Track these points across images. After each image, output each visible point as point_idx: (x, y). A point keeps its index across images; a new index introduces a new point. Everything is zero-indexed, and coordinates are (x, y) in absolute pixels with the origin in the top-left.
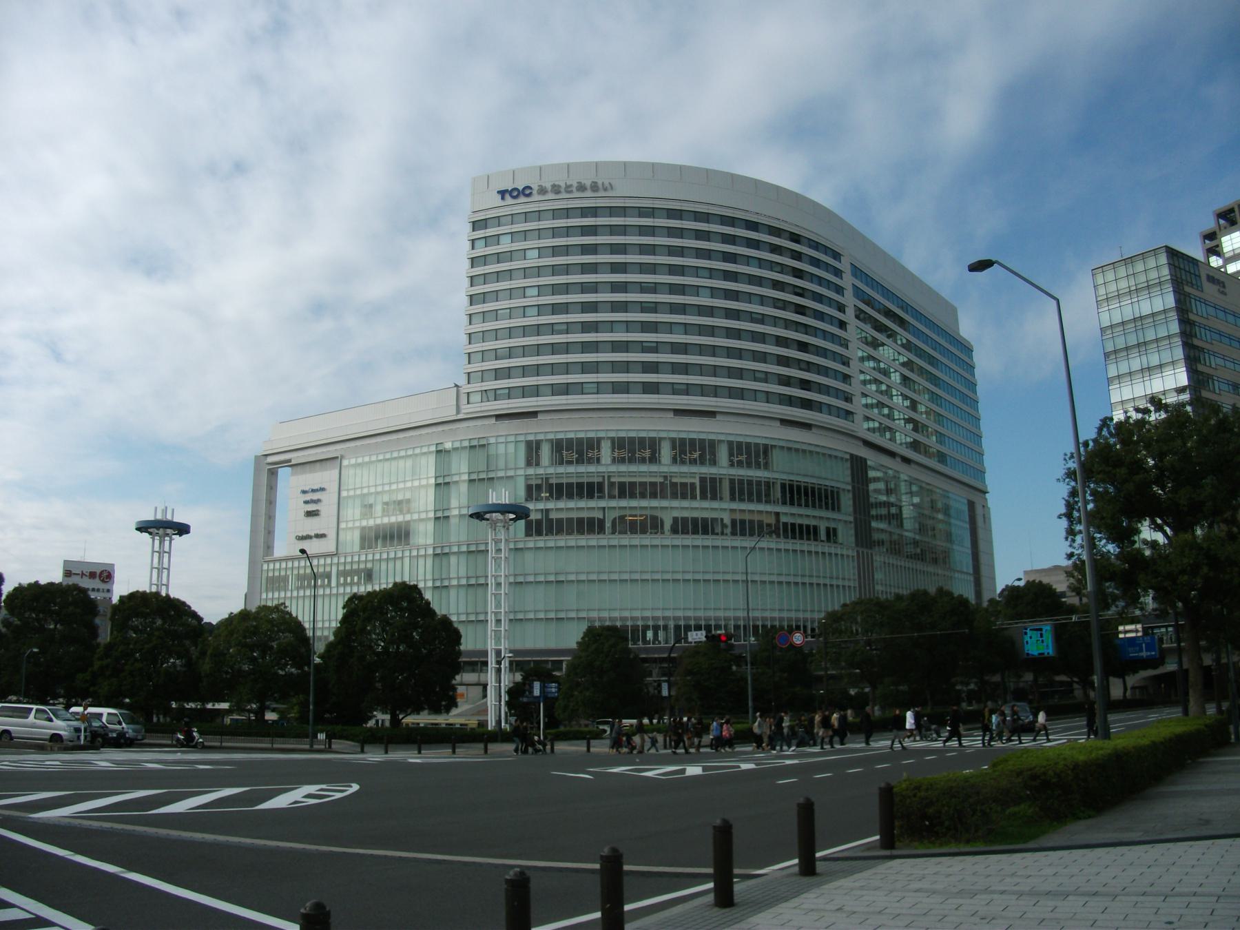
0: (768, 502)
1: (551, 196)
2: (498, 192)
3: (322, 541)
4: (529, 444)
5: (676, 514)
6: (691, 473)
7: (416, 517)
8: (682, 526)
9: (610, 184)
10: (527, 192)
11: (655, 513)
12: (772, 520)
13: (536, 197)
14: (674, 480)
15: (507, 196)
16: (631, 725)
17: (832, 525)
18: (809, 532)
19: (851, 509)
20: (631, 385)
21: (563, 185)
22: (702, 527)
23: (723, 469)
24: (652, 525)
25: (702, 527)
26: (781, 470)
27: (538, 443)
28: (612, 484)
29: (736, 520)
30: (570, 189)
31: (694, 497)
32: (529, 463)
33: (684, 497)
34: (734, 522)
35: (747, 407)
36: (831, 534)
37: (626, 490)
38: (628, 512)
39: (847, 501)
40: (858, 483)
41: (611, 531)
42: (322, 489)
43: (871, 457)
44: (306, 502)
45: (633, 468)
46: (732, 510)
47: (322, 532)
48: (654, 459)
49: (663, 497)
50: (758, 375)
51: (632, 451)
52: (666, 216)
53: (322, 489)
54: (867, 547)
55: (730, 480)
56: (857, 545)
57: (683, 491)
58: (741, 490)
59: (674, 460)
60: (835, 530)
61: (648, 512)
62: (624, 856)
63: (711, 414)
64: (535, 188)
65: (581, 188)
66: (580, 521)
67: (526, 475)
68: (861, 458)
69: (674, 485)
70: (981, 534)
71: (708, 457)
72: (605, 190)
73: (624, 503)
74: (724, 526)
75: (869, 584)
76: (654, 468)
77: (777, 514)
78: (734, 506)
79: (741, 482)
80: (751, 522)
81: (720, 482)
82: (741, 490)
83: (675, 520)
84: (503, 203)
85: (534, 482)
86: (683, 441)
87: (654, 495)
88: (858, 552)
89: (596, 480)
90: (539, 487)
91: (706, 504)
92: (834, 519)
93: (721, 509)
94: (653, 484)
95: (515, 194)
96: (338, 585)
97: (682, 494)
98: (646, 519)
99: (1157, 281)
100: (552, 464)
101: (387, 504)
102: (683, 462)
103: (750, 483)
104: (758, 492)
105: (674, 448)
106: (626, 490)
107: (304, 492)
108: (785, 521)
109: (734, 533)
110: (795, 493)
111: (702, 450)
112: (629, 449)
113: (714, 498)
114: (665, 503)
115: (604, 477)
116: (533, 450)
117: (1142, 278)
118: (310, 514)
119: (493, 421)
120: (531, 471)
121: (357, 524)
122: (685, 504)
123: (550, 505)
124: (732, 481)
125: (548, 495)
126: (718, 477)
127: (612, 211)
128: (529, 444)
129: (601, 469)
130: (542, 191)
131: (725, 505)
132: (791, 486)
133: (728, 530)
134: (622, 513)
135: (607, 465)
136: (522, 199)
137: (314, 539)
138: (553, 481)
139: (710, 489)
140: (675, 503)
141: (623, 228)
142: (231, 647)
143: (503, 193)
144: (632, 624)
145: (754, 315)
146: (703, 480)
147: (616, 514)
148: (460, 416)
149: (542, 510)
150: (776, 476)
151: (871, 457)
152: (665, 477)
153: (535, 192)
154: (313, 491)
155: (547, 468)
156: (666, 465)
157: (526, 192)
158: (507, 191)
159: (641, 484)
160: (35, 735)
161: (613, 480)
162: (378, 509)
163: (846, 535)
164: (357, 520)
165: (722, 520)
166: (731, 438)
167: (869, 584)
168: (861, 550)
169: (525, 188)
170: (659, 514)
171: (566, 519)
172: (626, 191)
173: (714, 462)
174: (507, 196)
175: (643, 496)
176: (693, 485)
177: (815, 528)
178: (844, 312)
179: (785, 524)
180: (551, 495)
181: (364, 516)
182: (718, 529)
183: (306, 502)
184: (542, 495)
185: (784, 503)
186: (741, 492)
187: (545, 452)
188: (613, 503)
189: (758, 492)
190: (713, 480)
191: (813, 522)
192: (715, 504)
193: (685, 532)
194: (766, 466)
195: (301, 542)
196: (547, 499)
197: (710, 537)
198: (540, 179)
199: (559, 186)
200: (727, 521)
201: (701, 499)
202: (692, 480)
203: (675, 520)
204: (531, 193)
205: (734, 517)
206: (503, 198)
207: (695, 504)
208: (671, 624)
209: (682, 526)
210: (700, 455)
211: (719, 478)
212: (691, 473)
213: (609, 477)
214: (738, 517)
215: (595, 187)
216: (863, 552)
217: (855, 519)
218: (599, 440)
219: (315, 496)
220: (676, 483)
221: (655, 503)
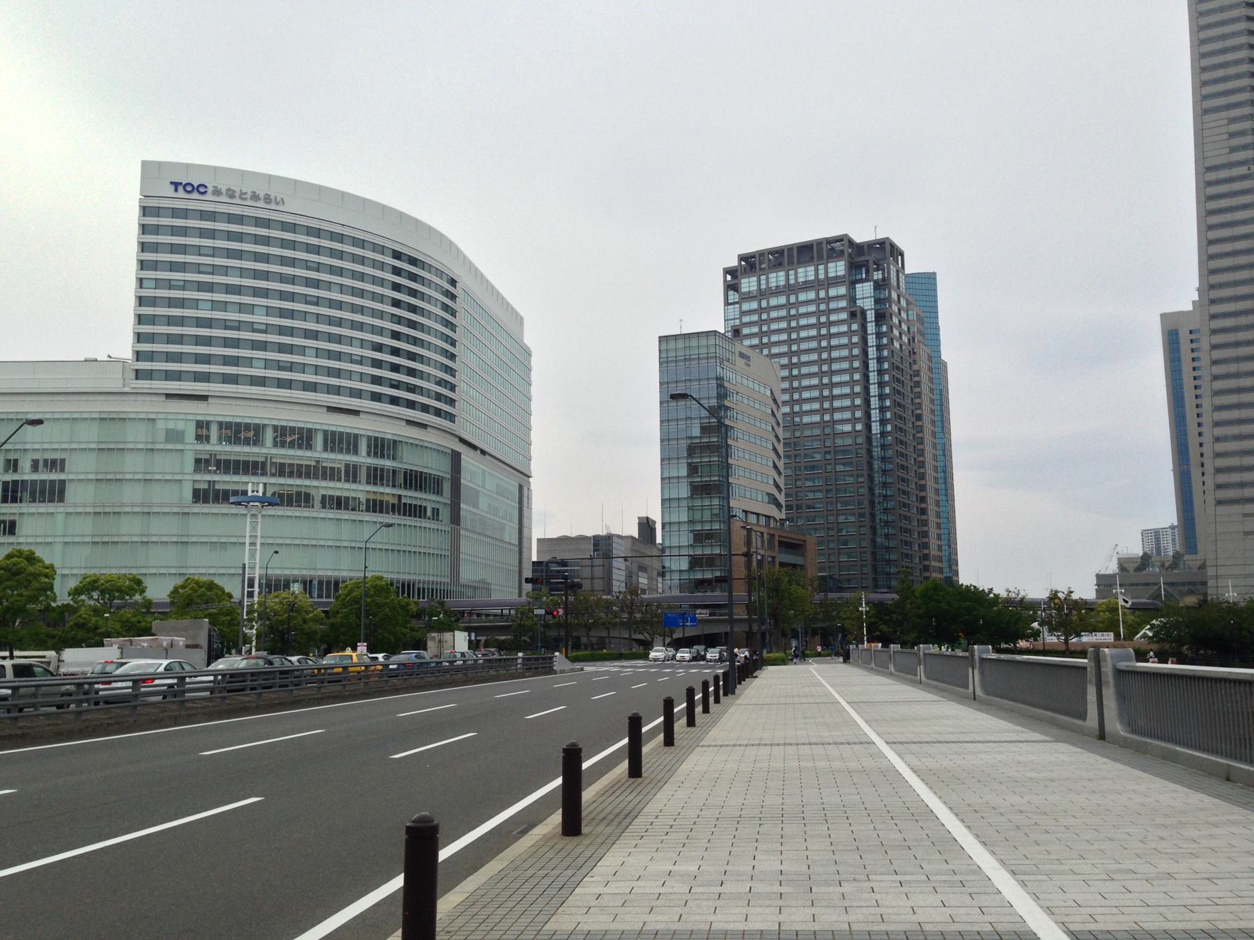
0: (394, 486)
1: (224, 199)
5: (323, 492)
6: (338, 459)
7: (72, 477)
9: (282, 199)
10: (202, 190)
11: (308, 491)
12: (396, 501)
13: (209, 197)
15: (180, 189)
18: (416, 511)
19: (449, 496)
20: (182, 373)
22: (339, 503)
23: (363, 459)
24: (303, 499)
25: (339, 503)
26: (410, 461)
30: (245, 197)
31: (339, 480)
33: (332, 479)
34: (368, 500)
36: (436, 512)
37: (282, 470)
39: (447, 488)
45: (237, 449)
49: (316, 478)
51: (237, 432)
56: (451, 523)
57: (330, 474)
58: (376, 476)
60: (438, 509)
62: (583, 750)
63: (356, 413)
65: (255, 197)
69: (324, 468)
72: (277, 203)
73: (282, 481)
76: (308, 453)
77: (400, 496)
79: (375, 469)
80: (381, 502)
82: (376, 476)
83: (324, 497)
84: (173, 194)
86: (284, 428)
87: (308, 476)
90: (207, 462)
91: (347, 486)
92: (425, 499)
93: (360, 490)
94: (308, 466)
97: (322, 475)
99: (674, 359)
102: (283, 445)
106: (282, 470)
109: (368, 510)
110: (415, 480)
111: (346, 442)
112: (285, 436)
113: (355, 481)
114: (315, 483)
115: (266, 458)
116: (202, 427)
117: (672, 354)
122: (332, 484)
124: (369, 468)
127: (285, 226)
128: (199, 424)
129: (264, 451)
130: (217, 192)
131: (361, 487)
133: (364, 507)
135: (213, 445)
136: (195, 195)
139: (351, 473)
140: (324, 484)
142: (566, 613)
143: (176, 185)
146: (347, 466)
148: (127, 389)
150: (400, 465)
152: (318, 462)
155: (216, 447)
156: (317, 453)
157: (200, 189)
158: (181, 184)
159: (289, 464)
160: (936, 687)
164: (707, 521)
169: (200, 185)
170: (313, 492)
172: (294, 208)
173: (356, 452)
174: (180, 189)
175: (300, 476)
178: (455, 347)
179: (405, 504)
185: (405, 488)
186: (375, 477)
190: (355, 466)
192: (354, 486)
193: (206, 501)
196: (215, 472)
198: (215, 180)
199: (234, 191)
200: (363, 500)
203: (324, 497)
204: (206, 192)
205: (369, 497)
206: (176, 190)
207: (339, 485)
210: (298, 439)
212: (338, 459)
215: (268, 199)
218: (264, 426)
220: (327, 467)
221: (307, 482)
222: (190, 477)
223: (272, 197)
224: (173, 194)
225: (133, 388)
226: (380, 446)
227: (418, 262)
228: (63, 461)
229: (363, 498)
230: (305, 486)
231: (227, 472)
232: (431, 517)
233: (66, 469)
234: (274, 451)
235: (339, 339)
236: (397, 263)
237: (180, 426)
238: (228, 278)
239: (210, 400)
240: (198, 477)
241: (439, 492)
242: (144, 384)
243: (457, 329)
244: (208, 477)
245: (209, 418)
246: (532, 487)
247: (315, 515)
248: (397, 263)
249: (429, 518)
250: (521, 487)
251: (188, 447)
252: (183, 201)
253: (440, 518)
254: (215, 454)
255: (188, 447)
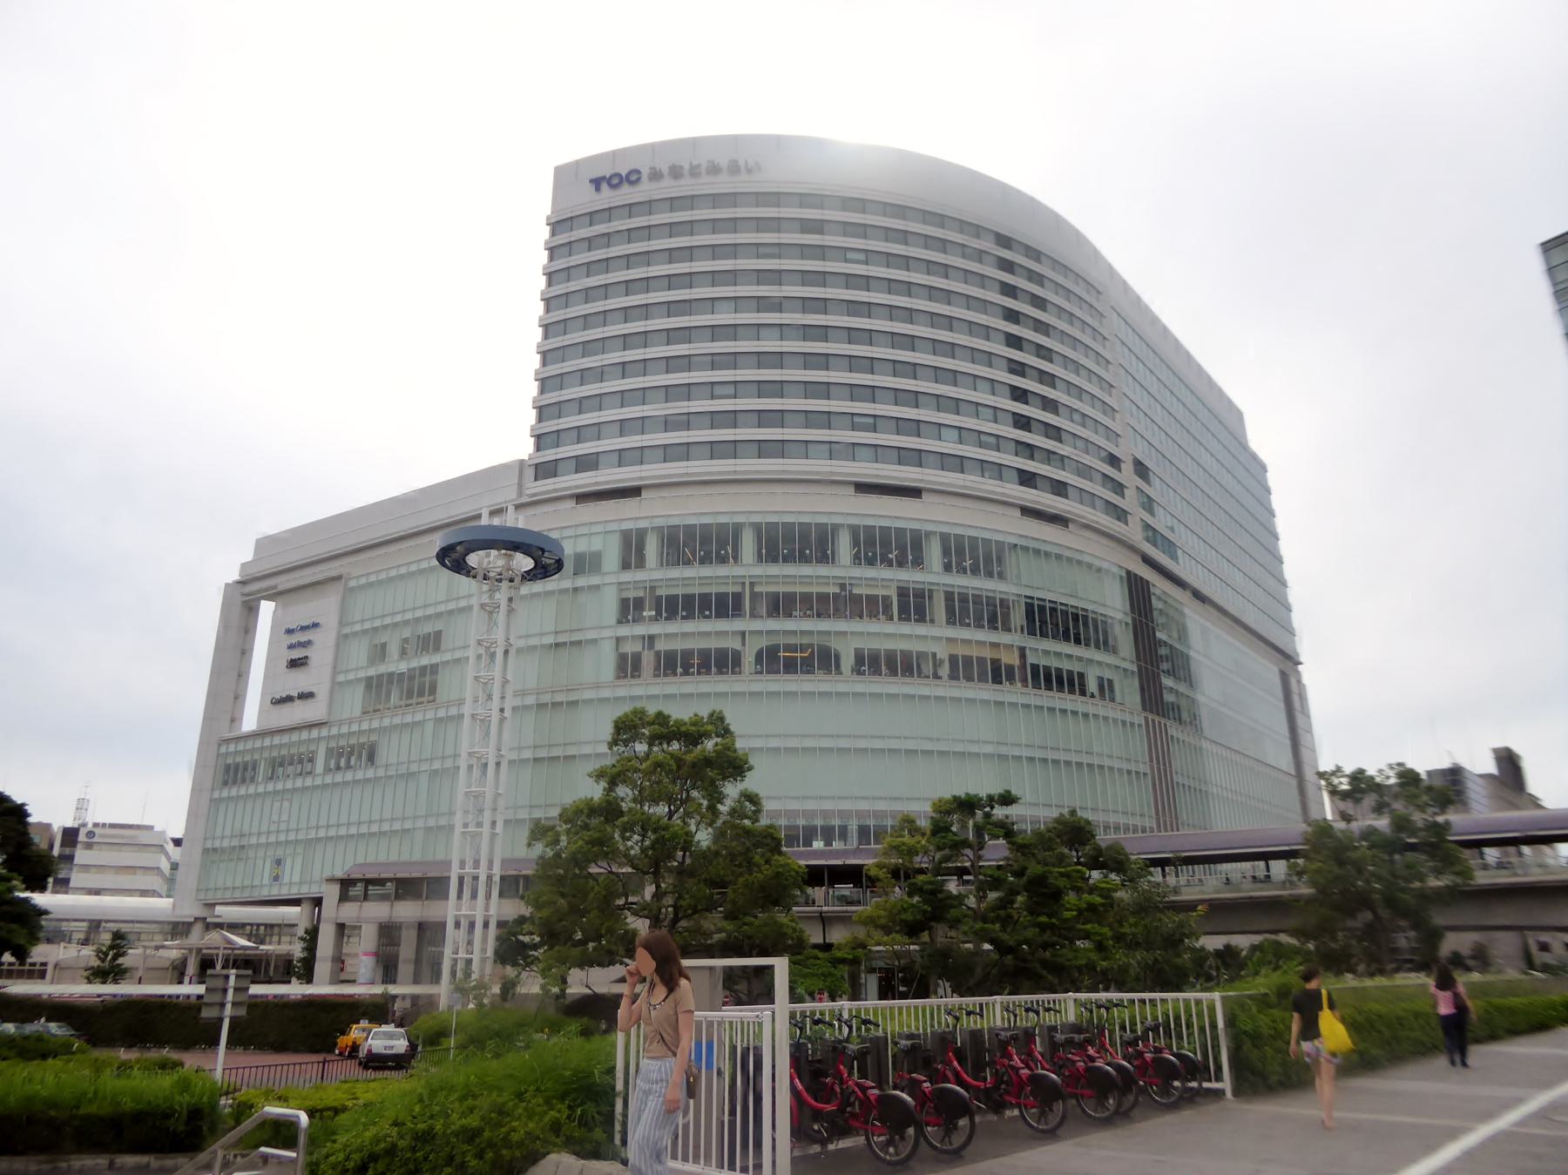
1: (667, 182)
2: (591, 181)
3: (309, 702)
4: (626, 536)
6: (884, 579)
7: (448, 657)
8: (869, 663)
10: (633, 178)
14: (856, 591)
15: (604, 186)
16: (907, 1046)
17: (1107, 674)
18: (1070, 683)
21: (687, 167)
22: (903, 665)
24: (823, 660)
25: (903, 665)
27: (641, 534)
28: (755, 596)
29: (957, 656)
32: (626, 566)
34: (953, 659)
35: (968, 484)
36: (1105, 688)
37: (780, 605)
38: (782, 641)
39: (1124, 639)
40: (1140, 615)
41: (753, 670)
42: (315, 625)
43: (1159, 584)
44: (291, 647)
46: (949, 640)
47: (306, 690)
48: (825, 557)
50: (967, 251)
52: (896, 461)
53: (315, 625)
54: (1164, 716)
55: (946, 593)
56: (1144, 709)
57: (873, 607)
58: (960, 609)
59: (857, 559)
61: (815, 640)
63: (914, 492)
64: (645, 172)
66: (705, 655)
67: (620, 583)
68: (1141, 578)
70: (1304, 739)
71: (910, 557)
74: (937, 664)
75: (1165, 771)
76: (822, 570)
78: (952, 632)
81: (930, 597)
85: (631, 594)
88: (1146, 719)
89: (731, 589)
90: (639, 604)
95: (615, 181)
96: (327, 770)
98: (812, 653)
100: (662, 565)
101: (406, 641)
103: (977, 599)
104: (993, 614)
105: (856, 543)
106: (780, 605)
107: (289, 631)
108: (1035, 662)
109: (954, 676)
113: (921, 618)
115: (744, 584)
118: (294, 664)
119: (570, 504)
120: (627, 577)
121: (362, 674)
123: (656, 629)
124: (949, 597)
125: (654, 613)
126: (927, 587)
128: (626, 536)
132: (1042, 609)
134: (772, 641)
136: (626, 188)
137: (298, 702)
138: (662, 592)
139: (913, 605)
141: (825, 387)
144: (787, 823)
145: (983, 438)
147: (764, 643)
149: (644, 637)
150: (1014, 590)
151: (1159, 584)
152: (843, 586)
153: (645, 177)
154: (304, 628)
155: (657, 574)
156: (844, 569)
157: (632, 178)
158: (603, 178)
161: (757, 589)
162: (394, 650)
163: (1129, 692)
165: (934, 655)
166: (945, 529)
167: (1165, 771)
168: (1150, 717)
170: (835, 644)
171: (634, 598)
173: (918, 562)
174: (604, 186)
176: (886, 599)
177: (1081, 676)
179: (1035, 668)
180: (659, 613)
181: (372, 662)
182: (928, 668)
183: (291, 647)
184: (645, 614)
186: (965, 612)
187: (652, 548)
188: (757, 625)
189: (993, 614)
190: (920, 594)
191: (1076, 668)
192: (921, 630)
194: (1001, 576)
195: (279, 706)
196: (656, 619)
197: (915, 680)
201: (900, 619)
202: (885, 592)
204: (638, 180)
206: (598, 189)
207: (890, 628)
208: (853, 826)
209: (869, 663)
211: (929, 590)
212: (884, 579)
213: (752, 584)
214: (961, 651)
216: (1160, 723)
217: (1140, 668)
219: (303, 637)
222: (608, 633)
223: (742, 164)
224: (596, 196)
225: (534, 495)
226: (961, 552)
227: (1016, 268)
228: (438, 634)
229: (943, 653)
230: (818, 632)
231: (672, 615)
232: (1096, 693)
233: (443, 647)
234: (759, 570)
235: (916, 427)
236: (1014, 329)
237: (596, 545)
238: (832, 432)
239: (644, 494)
240: (624, 631)
241: (1105, 644)
242: (548, 485)
243: (1126, 491)
244: (641, 630)
245: (643, 524)
246: (1306, 679)
247: (842, 688)
248: (1014, 329)
249: (1093, 696)
250: (1284, 677)
251: (608, 579)
252: (608, 197)
253: (1118, 698)
254: (653, 588)
255: (608, 579)
